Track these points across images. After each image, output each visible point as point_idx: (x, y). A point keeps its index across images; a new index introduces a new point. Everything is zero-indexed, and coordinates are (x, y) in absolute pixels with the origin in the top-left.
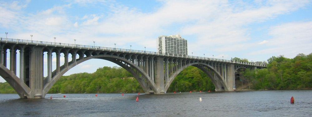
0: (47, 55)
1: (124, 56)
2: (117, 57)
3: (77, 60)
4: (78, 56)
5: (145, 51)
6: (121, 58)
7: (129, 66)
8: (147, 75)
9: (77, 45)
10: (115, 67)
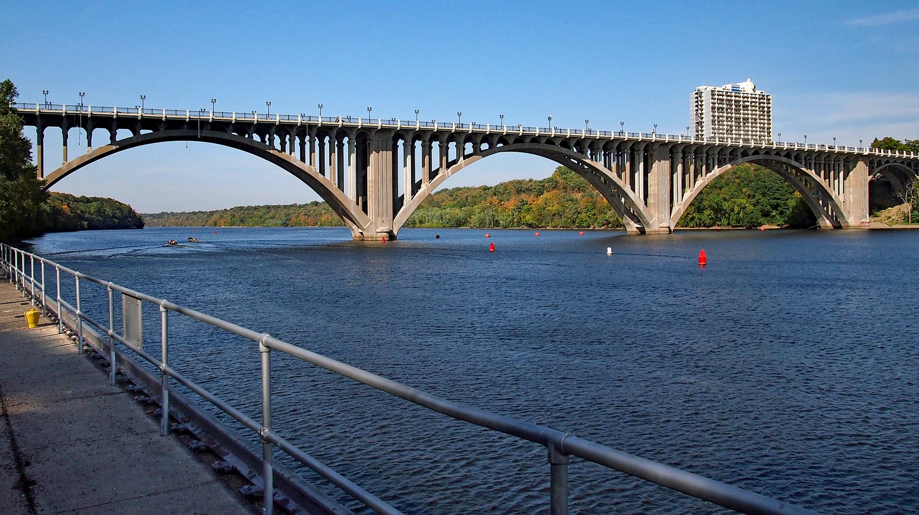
2: (557, 148)
7: (586, 167)
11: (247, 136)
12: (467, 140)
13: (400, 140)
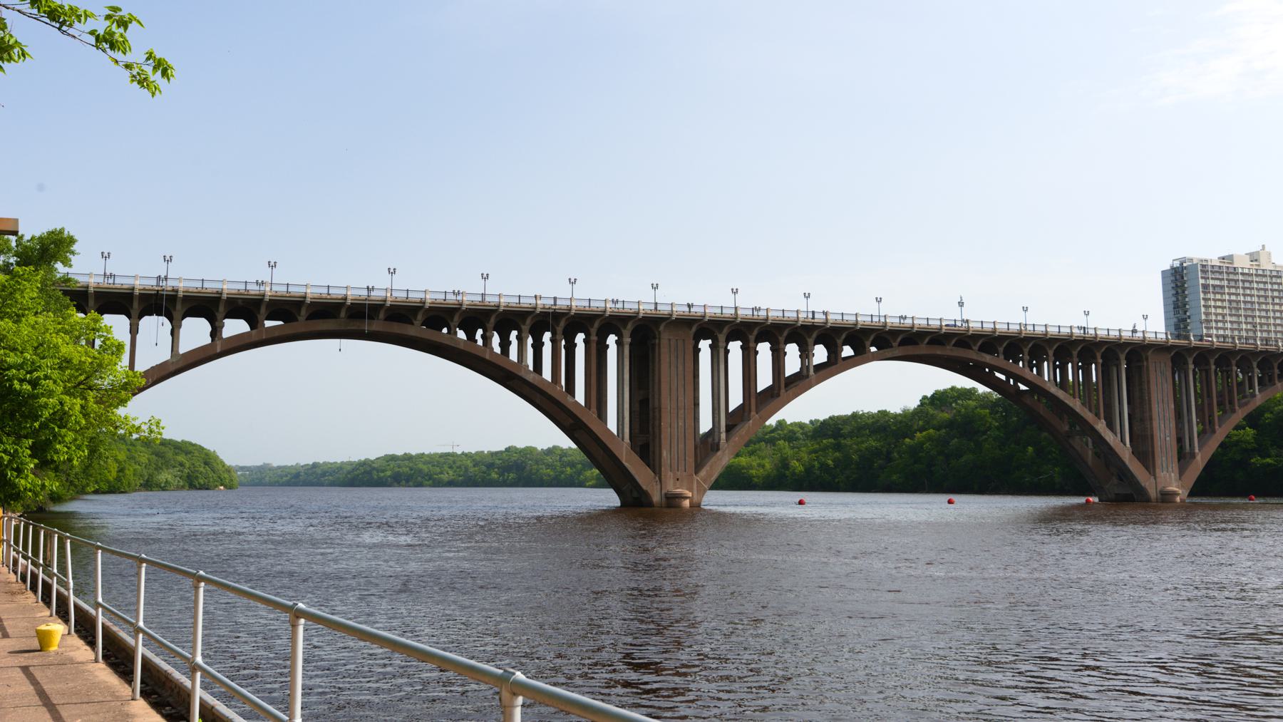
0: (740, 352)
1: (1001, 349)
2: (973, 355)
3: (815, 366)
4: (820, 354)
5: (1143, 332)
6: (987, 358)
7: (1023, 387)
8: (1101, 426)
9: (813, 312)
10: (974, 388)
11: (445, 330)
12: (732, 337)
13: (741, 344)
